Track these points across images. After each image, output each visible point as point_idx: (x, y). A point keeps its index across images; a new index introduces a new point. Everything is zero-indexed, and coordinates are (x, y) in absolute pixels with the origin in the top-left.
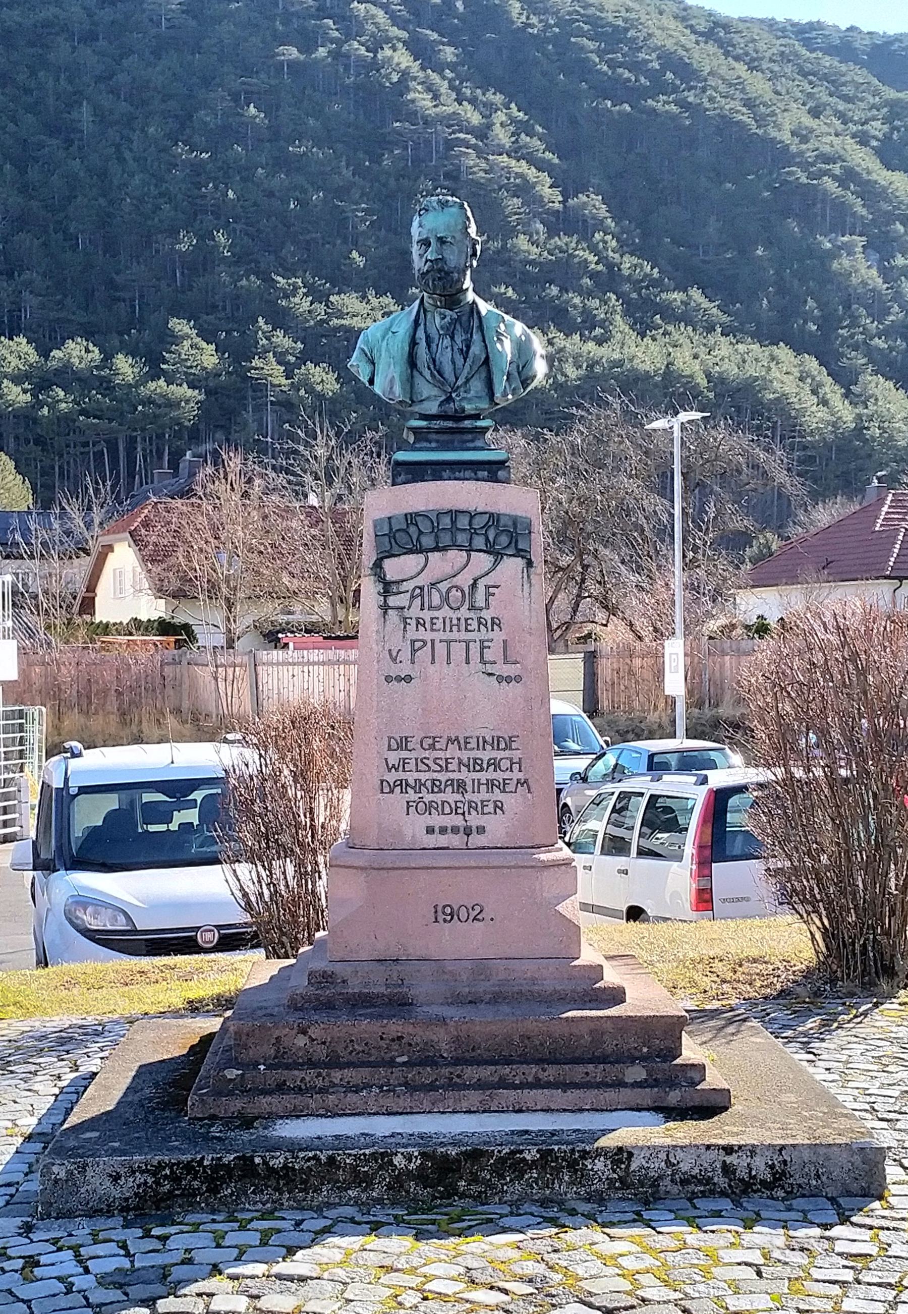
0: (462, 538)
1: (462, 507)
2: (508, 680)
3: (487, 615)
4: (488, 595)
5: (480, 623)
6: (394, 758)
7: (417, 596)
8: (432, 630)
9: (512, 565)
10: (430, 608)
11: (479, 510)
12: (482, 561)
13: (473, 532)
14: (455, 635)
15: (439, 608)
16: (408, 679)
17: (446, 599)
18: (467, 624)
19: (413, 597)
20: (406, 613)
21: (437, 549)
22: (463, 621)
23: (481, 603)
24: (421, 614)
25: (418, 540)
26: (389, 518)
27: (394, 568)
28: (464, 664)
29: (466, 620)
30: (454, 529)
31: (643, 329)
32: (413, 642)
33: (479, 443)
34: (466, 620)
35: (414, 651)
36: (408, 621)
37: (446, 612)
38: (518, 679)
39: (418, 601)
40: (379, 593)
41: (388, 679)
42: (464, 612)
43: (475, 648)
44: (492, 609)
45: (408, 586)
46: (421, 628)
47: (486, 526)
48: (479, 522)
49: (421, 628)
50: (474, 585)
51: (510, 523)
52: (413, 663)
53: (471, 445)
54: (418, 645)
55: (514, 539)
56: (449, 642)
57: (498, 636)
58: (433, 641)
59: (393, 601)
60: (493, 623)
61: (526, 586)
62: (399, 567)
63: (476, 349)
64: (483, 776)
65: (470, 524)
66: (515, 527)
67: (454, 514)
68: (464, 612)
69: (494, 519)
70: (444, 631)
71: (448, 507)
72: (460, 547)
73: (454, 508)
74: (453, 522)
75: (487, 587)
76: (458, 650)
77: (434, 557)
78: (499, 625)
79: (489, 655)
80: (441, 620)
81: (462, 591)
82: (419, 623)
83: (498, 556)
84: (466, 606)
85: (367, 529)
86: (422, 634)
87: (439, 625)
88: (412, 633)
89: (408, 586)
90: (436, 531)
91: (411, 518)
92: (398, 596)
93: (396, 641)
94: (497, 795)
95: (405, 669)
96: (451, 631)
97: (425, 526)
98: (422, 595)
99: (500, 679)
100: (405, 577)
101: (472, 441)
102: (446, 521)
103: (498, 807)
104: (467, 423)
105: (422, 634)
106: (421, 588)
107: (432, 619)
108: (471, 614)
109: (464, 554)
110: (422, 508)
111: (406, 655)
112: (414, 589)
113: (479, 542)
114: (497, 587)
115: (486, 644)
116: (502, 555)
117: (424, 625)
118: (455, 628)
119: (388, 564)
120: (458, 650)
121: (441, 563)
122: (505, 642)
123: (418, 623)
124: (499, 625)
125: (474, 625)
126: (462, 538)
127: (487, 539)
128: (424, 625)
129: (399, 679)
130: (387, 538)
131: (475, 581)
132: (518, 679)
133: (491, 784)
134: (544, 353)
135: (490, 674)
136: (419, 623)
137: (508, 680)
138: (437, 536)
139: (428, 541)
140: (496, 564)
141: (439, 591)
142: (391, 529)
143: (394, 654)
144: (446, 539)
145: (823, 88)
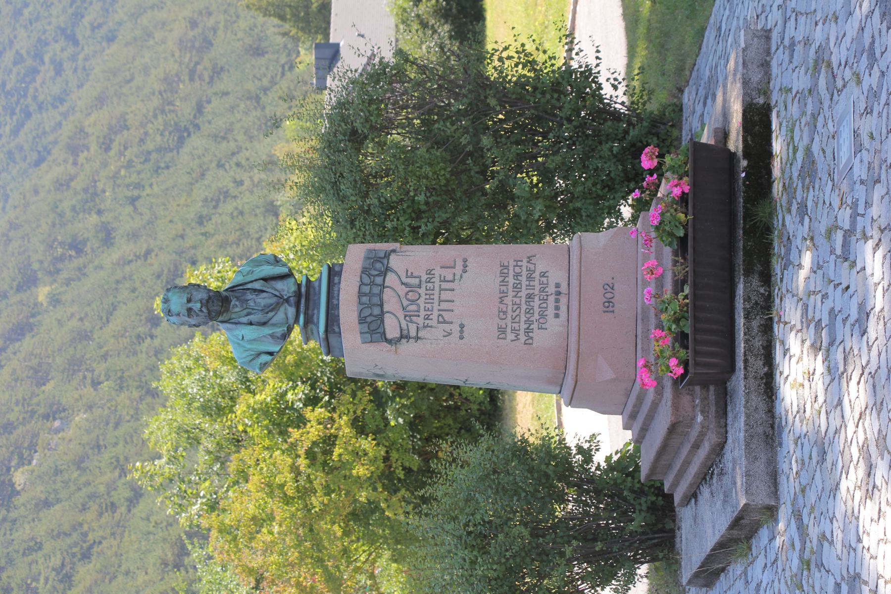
1: (357, 289)
3: (424, 277)
4: (412, 276)
5: (429, 282)
9: (394, 262)
10: (418, 311)
11: (359, 279)
12: (390, 279)
13: (372, 284)
14: (436, 297)
15: (418, 305)
16: (462, 326)
17: (413, 302)
19: (411, 322)
23: (417, 281)
26: (361, 333)
27: (392, 332)
30: (370, 294)
32: (439, 322)
33: (317, 284)
35: (445, 322)
37: (421, 302)
38: (465, 260)
39: (414, 318)
41: (461, 338)
42: (422, 291)
47: (369, 276)
48: (366, 280)
51: (368, 261)
53: (317, 288)
54: (441, 319)
56: (440, 301)
57: (438, 272)
58: (439, 310)
59: (413, 333)
60: (429, 274)
63: (257, 285)
65: (367, 285)
67: (361, 294)
69: (365, 271)
71: (356, 299)
72: (382, 292)
74: (366, 295)
76: (445, 295)
77: (386, 308)
82: (427, 318)
83: (388, 269)
88: (433, 323)
91: (362, 320)
95: (456, 328)
101: (314, 289)
102: (365, 299)
104: (303, 290)
106: (405, 316)
108: (423, 286)
109: (385, 290)
111: (447, 327)
113: (379, 280)
118: (432, 297)
120: (445, 295)
121: (391, 303)
123: (427, 319)
125: (430, 285)
126: (376, 290)
129: (462, 332)
131: (402, 283)
132: (465, 260)
135: (461, 277)
136: (427, 318)
137: (465, 266)
138: (374, 305)
139: (376, 311)
144: (376, 300)
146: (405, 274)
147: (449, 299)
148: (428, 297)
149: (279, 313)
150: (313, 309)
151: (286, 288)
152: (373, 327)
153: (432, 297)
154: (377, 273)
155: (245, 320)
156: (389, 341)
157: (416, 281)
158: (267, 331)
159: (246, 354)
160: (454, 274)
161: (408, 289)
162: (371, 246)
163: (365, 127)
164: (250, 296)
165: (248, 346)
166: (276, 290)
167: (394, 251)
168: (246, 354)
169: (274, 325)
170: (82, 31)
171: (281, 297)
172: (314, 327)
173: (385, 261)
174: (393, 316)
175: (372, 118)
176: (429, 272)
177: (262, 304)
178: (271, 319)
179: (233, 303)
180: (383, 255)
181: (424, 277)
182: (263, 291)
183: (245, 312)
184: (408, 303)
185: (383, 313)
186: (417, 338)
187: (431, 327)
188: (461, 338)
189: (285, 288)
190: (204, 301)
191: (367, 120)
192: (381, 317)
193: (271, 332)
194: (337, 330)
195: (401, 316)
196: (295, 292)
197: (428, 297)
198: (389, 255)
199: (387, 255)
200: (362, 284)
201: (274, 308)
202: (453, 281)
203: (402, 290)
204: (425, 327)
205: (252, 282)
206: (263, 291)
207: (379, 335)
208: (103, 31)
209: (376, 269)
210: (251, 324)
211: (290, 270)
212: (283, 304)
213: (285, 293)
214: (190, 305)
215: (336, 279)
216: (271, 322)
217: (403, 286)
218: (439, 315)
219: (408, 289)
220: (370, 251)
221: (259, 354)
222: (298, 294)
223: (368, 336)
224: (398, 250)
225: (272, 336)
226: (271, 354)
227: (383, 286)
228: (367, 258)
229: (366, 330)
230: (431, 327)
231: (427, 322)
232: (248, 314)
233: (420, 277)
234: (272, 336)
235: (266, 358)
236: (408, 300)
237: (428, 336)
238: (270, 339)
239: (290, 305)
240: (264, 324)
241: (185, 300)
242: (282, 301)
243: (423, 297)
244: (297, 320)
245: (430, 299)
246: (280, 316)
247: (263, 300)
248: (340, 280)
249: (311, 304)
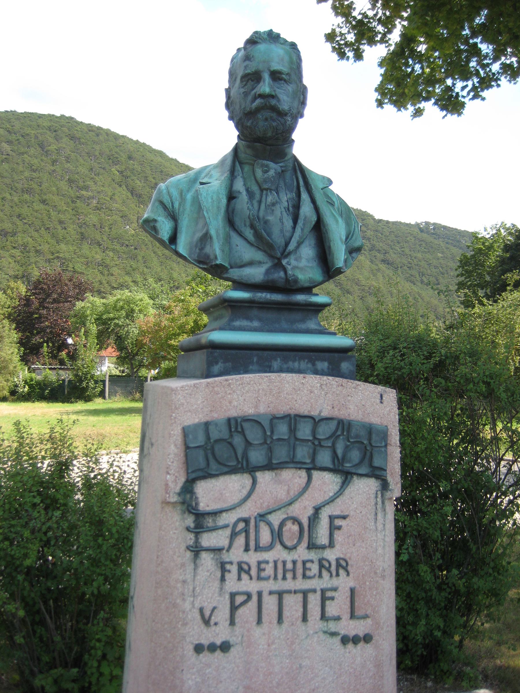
1: (304, 410)
2: (355, 640)
3: (331, 555)
4: (333, 528)
5: (321, 566)
7: (240, 533)
8: (259, 578)
9: (364, 488)
10: (258, 548)
11: (325, 414)
12: (326, 482)
13: (316, 444)
14: (289, 584)
15: (270, 547)
16: (225, 647)
17: (278, 535)
18: (305, 569)
19: (234, 535)
20: (226, 557)
21: (269, 467)
22: (299, 566)
23: (322, 538)
24: (245, 557)
25: (245, 455)
26: (207, 424)
27: (210, 493)
28: (299, 622)
29: (304, 563)
30: (293, 440)
32: (233, 596)
33: (312, 325)
34: (304, 563)
35: (234, 608)
36: (228, 567)
37: (278, 553)
38: (367, 638)
39: (240, 540)
40: (188, 529)
41: (199, 649)
42: (302, 553)
43: (314, 600)
44: (337, 547)
45: (229, 518)
46: (244, 576)
47: (334, 437)
48: (324, 431)
49: (244, 576)
51: (363, 433)
52: (232, 623)
53: (303, 326)
54: (239, 599)
56: (280, 594)
57: (344, 583)
58: (260, 594)
59: (208, 540)
60: (339, 565)
61: (380, 516)
63: (306, 209)
65: (314, 432)
66: (370, 440)
67: (293, 420)
69: (344, 426)
70: (276, 578)
71: (283, 409)
72: (298, 465)
73: (292, 412)
74: (293, 430)
75: (332, 518)
76: (293, 605)
77: (264, 478)
78: (346, 569)
79: (332, 609)
80: (271, 565)
81: (300, 525)
82: (243, 569)
83: (347, 476)
84: (304, 544)
86: (249, 585)
87: (269, 570)
88: (232, 584)
89: (229, 518)
90: (269, 443)
91: (236, 425)
92: (214, 534)
95: (220, 633)
96: (284, 578)
98: (247, 531)
99: (345, 640)
100: (225, 506)
101: (303, 321)
102: (283, 429)
104: (300, 298)
105: (249, 585)
106: (246, 521)
107: (259, 563)
108: (313, 555)
109: (303, 474)
110: (249, 410)
111: (222, 615)
112: (235, 524)
113: (324, 458)
114: (344, 517)
115: (329, 594)
116: (352, 474)
117: (248, 572)
118: (289, 575)
120: (293, 605)
121: (275, 487)
122: (352, 591)
123: (240, 569)
124: (346, 569)
125: (314, 568)
126: (302, 453)
127: (335, 453)
128: (248, 572)
129: (212, 648)
130: (201, 452)
131: (317, 510)
132: (367, 638)
134: (75, 431)
135: (333, 634)
136: (243, 569)
137: (355, 640)
138: (270, 450)
139: (256, 456)
140: (344, 484)
141: (269, 524)
142: (208, 438)
143: (207, 614)
144: (281, 453)
146: (337, 513)
147: (286, 613)
148: (289, 566)
149: (253, 250)
150: (260, 320)
151: (303, 264)
152: (222, 451)
153: (289, 575)
154: (340, 452)
155: (239, 185)
156: (188, 488)
157: (322, 538)
158: (216, 225)
159: (175, 193)
160: (338, 619)
161: (305, 522)
162: (395, 437)
163: (461, 377)
164: (286, 198)
165: (189, 197)
166: (299, 244)
167: (385, 486)
168: (175, 193)
169: (228, 239)
170: (374, 253)
171: (285, 254)
172: (225, 320)
173: (363, 470)
174: (245, 492)
175: (471, 385)
176: (342, 565)
177: (270, 218)
178: (240, 234)
179: (272, 165)
180: (377, 463)
181: (331, 555)
182: (295, 221)
183: (255, 188)
184: (276, 524)
185: (252, 470)
186: (196, 550)
187: (223, 579)
188: (199, 649)
189: (303, 263)
190: (273, 102)
191: (468, 381)
192: (244, 467)
193: (213, 232)
194: (216, 369)
195: (243, 512)
196: (296, 281)
197: (289, 566)
198: (377, 477)
199: (378, 473)
200: (317, 422)
201: (262, 242)
202: (323, 617)
203: (303, 510)
204: (223, 567)
205: (313, 201)
206: (295, 221)
207: (202, 463)
208: (374, 259)
209: (347, 450)
210: (231, 197)
211: (339, 271)
212: (272, 257)
213: (293, 262)
214: (266, 76)
215: (323, 365)
216: (233, 234)
217: (310, 512)
218: (249, 596)
219: (305, 522)
220: (384, 435)
221: (174, 217)
222: (291, 287)
223: (201, 440)
224: (388, 494)
225: (206, 238)
226: (173, 239)
227: (311, 467)
228: (370, 430)
229: (215, 435)
230: (223, 579)
231: (234, 569)
232: (250, 194)
233: (331, 545)
234: (206, 238)
235: (165, 228)
236: (282, 524)
237: (203, 574)
238: (199, 235)
239: (267, 272)
240: (230, 221)
241: (276, 67)
242: (277, 255)
243: (288, 557)
244: (239, 285)
245: (284, 571)
246: (246, 252)
247: (279, 220)
248: (322, 373)
249: (270, 315)
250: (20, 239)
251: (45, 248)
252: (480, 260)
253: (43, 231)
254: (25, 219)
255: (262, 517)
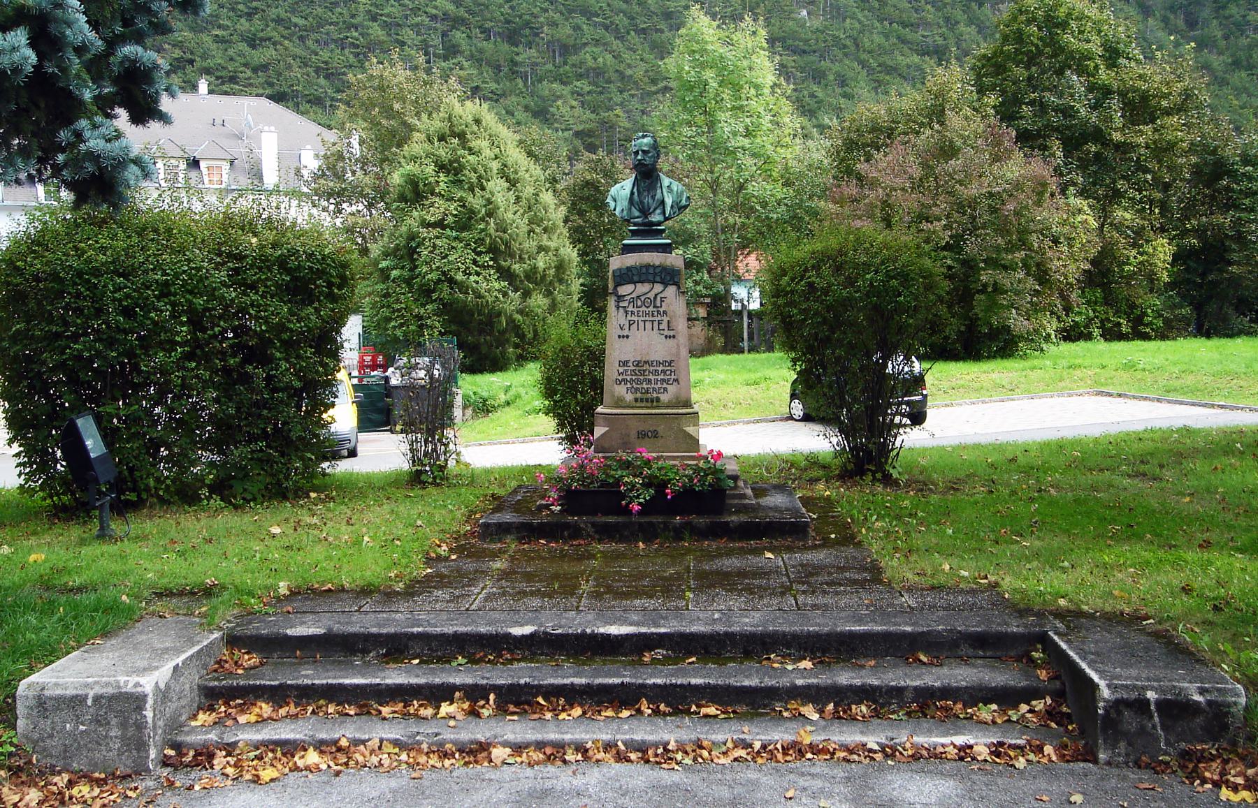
0: (651, 278)
6: (621, 370)
9: (671, 290)
12: (658, 287)
13: (655, 274)
31: (878, 86)
37: (644, 308)
42: (651, 309)
48: (657, 270)
50: (655, 298)
55: (672, 278)
57: (665, 319)
59: (621, 304)
62: (625, 290)
64: (659, 378)
68: (651, 309)
72: (649, 282)
76: (649, 325)
82: (633, 313)
85: (610, 274)
90: (640, 274)
93: (623, 321)
94: (665, 385)
97: (651, 271)
103: (665, 389)
113: (658, 279)
119: (619, 289)
120: (649, 325)
121: (642, 288)
126: (651, 278)
133: (663, 380)
136: (633, 313)
139: (636, 278)
145: (222, 608)
176: (665, 312)
186: (618, 308)
192: (631, 282)
203: (651, 295)
204: (626, 312)
250: (587, 56)
251: (639, 72)
252: (235, 290)
253: (633, 37)
254: (598, 16)
255: (638, 297)
